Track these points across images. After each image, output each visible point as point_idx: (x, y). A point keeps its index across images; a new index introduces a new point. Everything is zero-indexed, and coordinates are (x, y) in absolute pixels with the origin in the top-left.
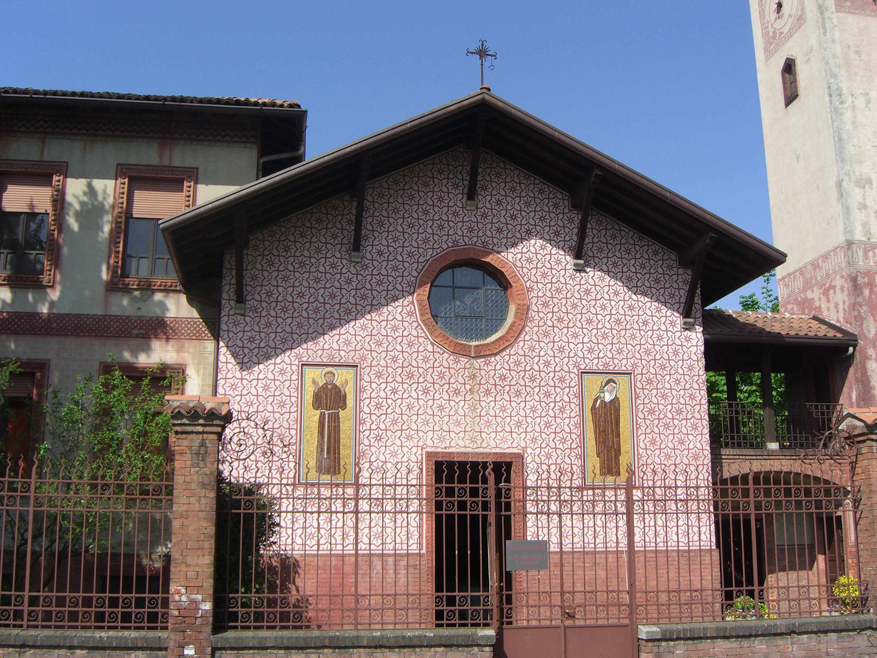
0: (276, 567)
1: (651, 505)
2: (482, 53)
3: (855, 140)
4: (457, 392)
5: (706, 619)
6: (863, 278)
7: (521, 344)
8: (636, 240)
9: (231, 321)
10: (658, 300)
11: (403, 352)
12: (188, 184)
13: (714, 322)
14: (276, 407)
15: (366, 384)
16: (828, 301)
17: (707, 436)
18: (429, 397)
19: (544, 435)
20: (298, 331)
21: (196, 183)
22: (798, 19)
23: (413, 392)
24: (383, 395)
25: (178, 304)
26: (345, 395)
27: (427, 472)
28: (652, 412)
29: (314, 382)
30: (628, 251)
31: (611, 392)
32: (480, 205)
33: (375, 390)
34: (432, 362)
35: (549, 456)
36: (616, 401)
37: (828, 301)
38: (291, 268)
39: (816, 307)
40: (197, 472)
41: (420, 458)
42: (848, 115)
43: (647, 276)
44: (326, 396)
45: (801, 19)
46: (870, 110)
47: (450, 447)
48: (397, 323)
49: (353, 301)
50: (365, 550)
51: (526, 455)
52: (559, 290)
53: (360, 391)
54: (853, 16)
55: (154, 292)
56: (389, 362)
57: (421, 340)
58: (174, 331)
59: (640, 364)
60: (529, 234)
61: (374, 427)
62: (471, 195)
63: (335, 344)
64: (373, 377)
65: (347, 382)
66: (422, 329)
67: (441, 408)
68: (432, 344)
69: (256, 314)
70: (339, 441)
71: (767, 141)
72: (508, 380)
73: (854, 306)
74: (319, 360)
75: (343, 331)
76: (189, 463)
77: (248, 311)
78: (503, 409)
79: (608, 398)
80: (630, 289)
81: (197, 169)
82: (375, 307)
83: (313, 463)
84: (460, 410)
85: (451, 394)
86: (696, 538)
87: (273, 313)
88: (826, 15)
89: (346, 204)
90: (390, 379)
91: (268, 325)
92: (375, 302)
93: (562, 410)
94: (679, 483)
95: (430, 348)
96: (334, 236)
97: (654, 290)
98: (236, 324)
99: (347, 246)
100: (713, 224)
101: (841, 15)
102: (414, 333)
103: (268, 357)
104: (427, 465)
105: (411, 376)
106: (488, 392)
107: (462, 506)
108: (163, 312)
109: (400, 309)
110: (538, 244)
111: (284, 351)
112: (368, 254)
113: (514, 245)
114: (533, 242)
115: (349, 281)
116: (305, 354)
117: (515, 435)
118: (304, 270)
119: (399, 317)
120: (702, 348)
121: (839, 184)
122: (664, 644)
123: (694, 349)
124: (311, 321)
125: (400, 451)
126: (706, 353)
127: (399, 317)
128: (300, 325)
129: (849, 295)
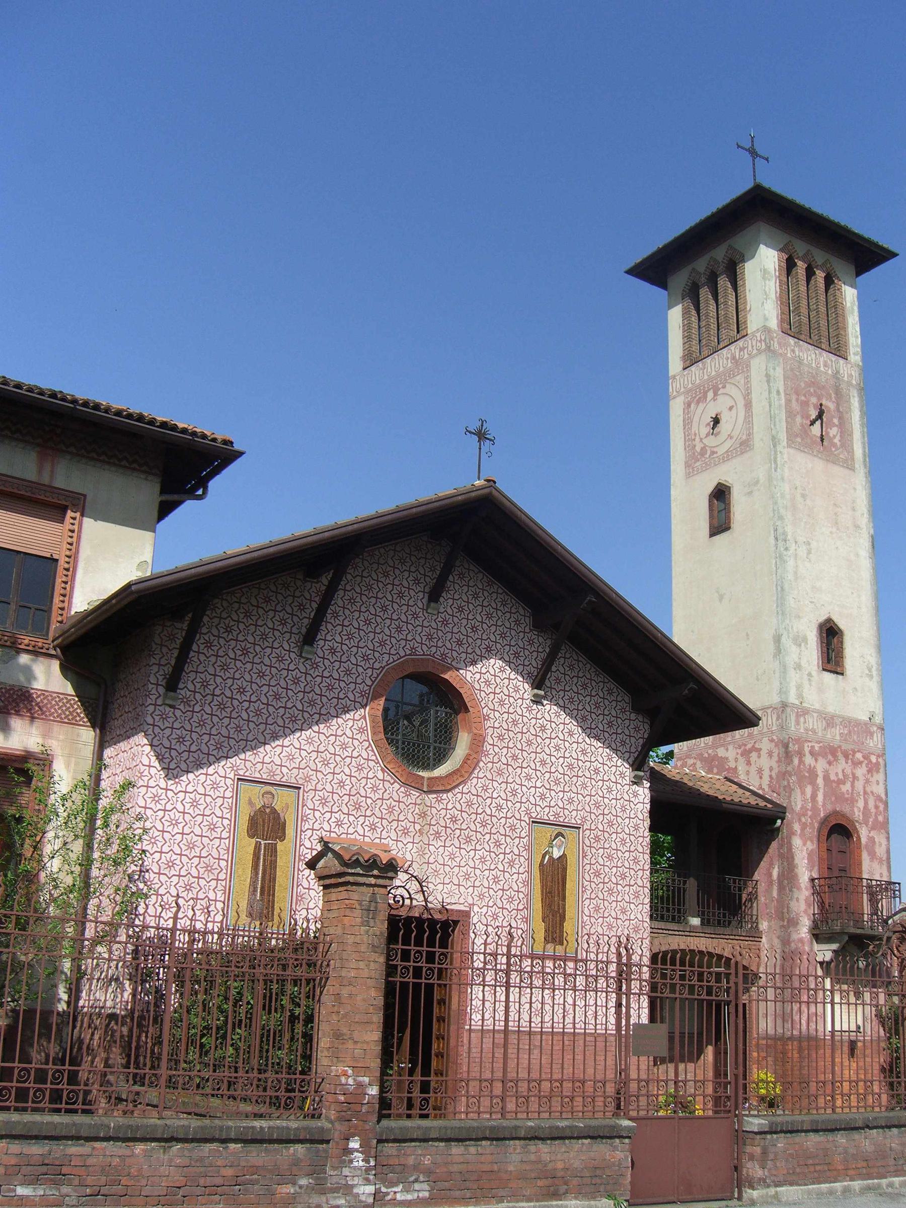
1: (562, 980)
2: (481, 435)
3: (796, 592)
4: (406, 832)
5: (519, 1116)
6: (794, 745)
8: (593, 674)
9: (157, 712)
10: (609, 747)
12: (73, 515)
13: (657, 780)
15: (308, 812)
16: (749, 763)
17: (648, 907)
21: (82, 515)
22: (741, 444)
25: (48, 673)
26: (285, 823)
28: (597, 874)
29: (250, 803)
30: (584, 686)
31: (559, 848)
35: (495, 917)
36: (564, 856)
37: (749, 763)
39: (730, 768)
42: (791, 563)
43: (601, 717)
45: (745, 445)
46: (810, 561)
50: (526, 1027)
51: (472, 914)
53: (302, 820)
54: (802, 454)
55: (19, 651)
57: (371, 764)
58: (39, 707)
59: (588, 818)
60: (488, 652)
66: (373, 751)
68: (382, 770)
71: (676, 570)
75: (286, 742)
76: (359, 920)
78: (452, 857)
79: (556, 854)
80: (584, 730)
81: (85, 496)
82: (324, 717)
83: (244, 905)
87: (208, 709)
88: (779, 448)
89: (299, 583)
92: (323, 711)
93: (511, 863)
96: (283, 622)
97: (606, 735)
99: (297, 637)
100: (699, 676)
101: (792, 451)
102: (365, 755)
103: (199, 765)
107: (417, 972)
108: (29, 682)
109: (350, 723)
110: (497, 665)
111: (218, 760)
112: (319, 650)
113: (474, 663)
114: (492, 661)
116: (242, 766)
120: (648, 806)
121: (777, 639)
122: (769, 1136)
123: (640, 806)
126: (652, 813)
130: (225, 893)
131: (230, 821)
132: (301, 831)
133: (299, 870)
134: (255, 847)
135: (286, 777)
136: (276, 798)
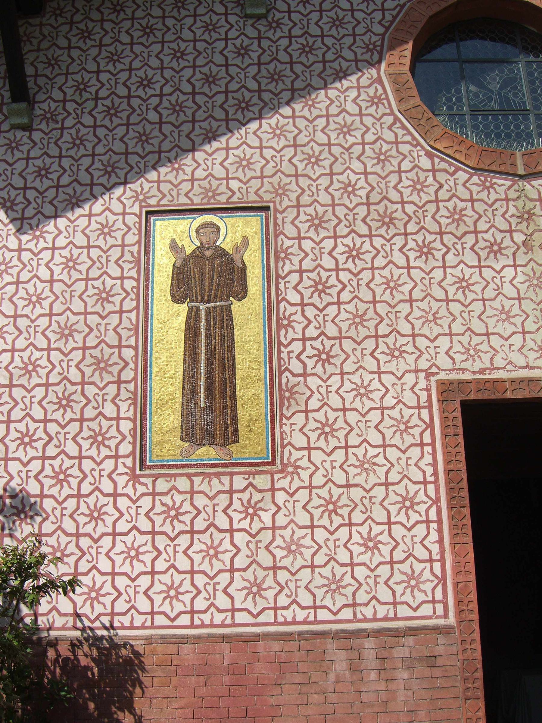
0: (87, 668)
4: (495, 249)
11: (366, 173)
14: (90, 302)
18: (432, 263)
24: (328, 262)
26: (244, 269)
27: (444, 427)
29: (174, 246)
33: (312, 253)
34: (432, 190)
38: (125, 38)
41: (424, 396)
44: (202, 272)
47: (493, 368)
48: (349, 119)
49: (254, 86)
53: (277, 258)
56: (337, 195)
57: (405, 148)
61: (311, 332)
63: (217, 167)
64: (304, 227)
65: (246, 242)
66: (404, 127)
67: (464, 285)
69: (52, 125)
70: (232, 369)
74: (183, 200)
77: (37, 121)
84: (507, 285)
90: (342, 230)
91: (78, 142)
95: (426, 163)
103: (75, 202)
104: (442, 411)
105: (388, 221)
116: (154, 191)
119: (351, 108)
124: (167, 129)
125: (376, 384)
127: (351, 108)
128: (144, 138)
130: (135, 404)
131: (138, 280)
132: (278, 276)
133: (280, 343)
134: (189, 317)
135: (238, 195)
136: (223, 231)
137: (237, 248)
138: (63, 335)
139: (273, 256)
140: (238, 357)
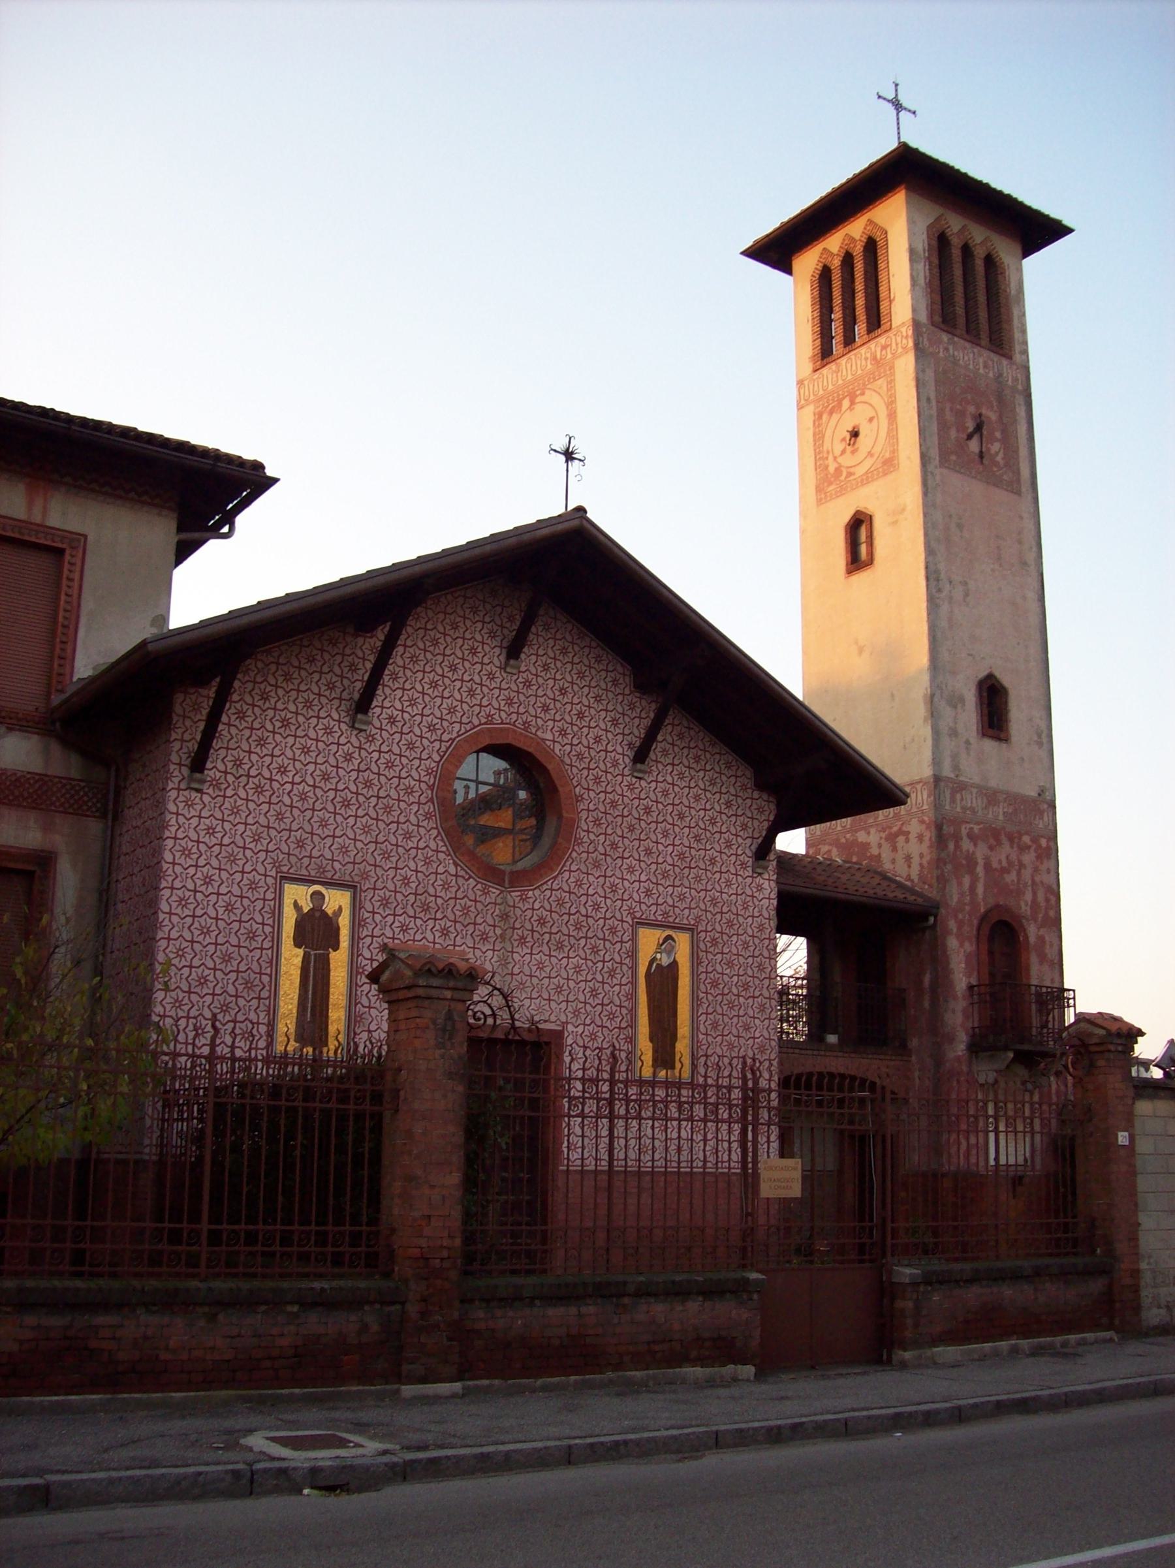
2: (569, 455)
4: (484, 938)
7: (566, 875)
14: (243, 938)
16: (895, 849)
19: (588, 1007)
20: (276, 825)
23: (428, 931)
26: (338, 929)
29: (296, 904)
32: (523, 669)
37: (895, 849)
40: (442, 1056)
52: (614, 804)
57: (442, 856)
62: (514, 651)
68: (456, 865)
72: (549, 925)
73: (939, 862)
74: (304, 872)
76: (432, 1042)
81: (85, 537)
85: (477, 939)
86: (726, 1158)
94: (710, 1081)
95: (452, 869)
98: (189, 804)
99: (348, 703)
101: (945, 471)
102: (433, 845)
106: (522, 940)
115: (348, 758)
117: (553, 1005)
118: (288, 732)
119: (413, 819)
120: (775, 902)
127: (413, 819)
129: (930, 847)
131: (273, 927)
137: (334, 913)
138: (224, 960)
139: (357, 923)
140: (331, 990)
